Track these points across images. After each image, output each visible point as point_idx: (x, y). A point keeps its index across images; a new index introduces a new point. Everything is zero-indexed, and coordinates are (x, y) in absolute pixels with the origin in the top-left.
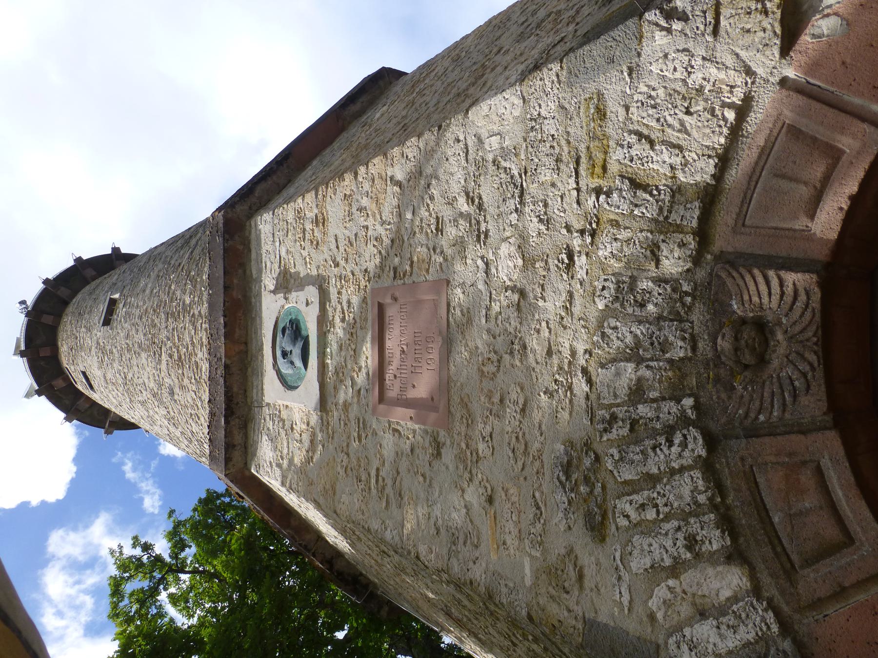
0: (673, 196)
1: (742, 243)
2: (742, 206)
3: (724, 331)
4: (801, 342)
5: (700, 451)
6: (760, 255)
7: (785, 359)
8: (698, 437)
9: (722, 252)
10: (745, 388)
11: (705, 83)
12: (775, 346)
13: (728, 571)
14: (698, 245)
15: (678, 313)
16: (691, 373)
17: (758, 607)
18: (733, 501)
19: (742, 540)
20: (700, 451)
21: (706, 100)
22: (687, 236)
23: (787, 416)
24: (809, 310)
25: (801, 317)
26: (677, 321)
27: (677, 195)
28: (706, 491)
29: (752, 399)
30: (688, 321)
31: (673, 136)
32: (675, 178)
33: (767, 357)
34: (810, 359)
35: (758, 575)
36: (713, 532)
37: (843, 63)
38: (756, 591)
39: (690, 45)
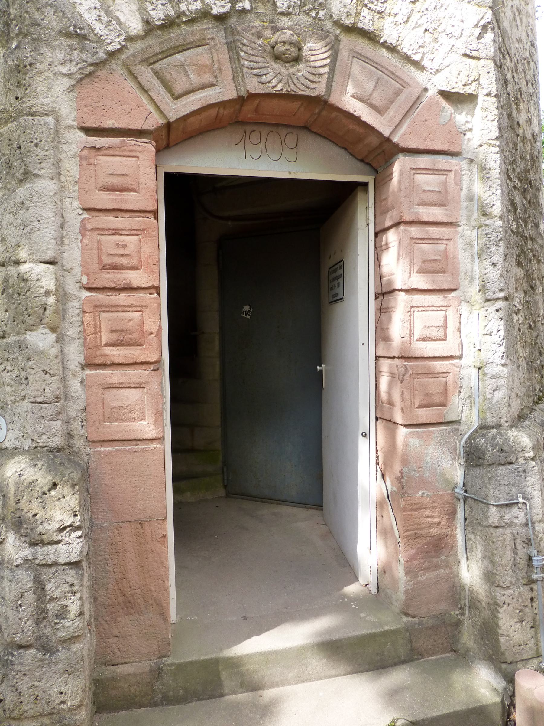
0: (379, 13)
1: (344, 54)
2: (365, 57)
3: (295, 36)
4: (288, 82)
5: (215, 9)
6: (336, 64)
7: (278, 72)
8: (224, 9)
9: (340, 41)
10: (260, 45)
11: (439, 44)
12: (285, 67)
13: (138, 21)
14: (347, 26)
15: (305, 5)
16: (266, 9)
17: (120, 38)
18: (184, 29)
19: (160, 32)
20: (215, 9)
21: (429, 44)
22: (353, 19)
23: (245, 70)
24: (305, 89)
25: (302, 84)
26: (300, 3)
27: (379, 15)
28: (188, 10)
29: (254, 49)
30: (300, 11)
31: (415, 18)
32: (389, 16)
33: (278, 61)
34: (279, 86)
35: (139, 41)
36: (162, 12)
37: (426, 120)
38: (130, 39)
39: (464, 38)
